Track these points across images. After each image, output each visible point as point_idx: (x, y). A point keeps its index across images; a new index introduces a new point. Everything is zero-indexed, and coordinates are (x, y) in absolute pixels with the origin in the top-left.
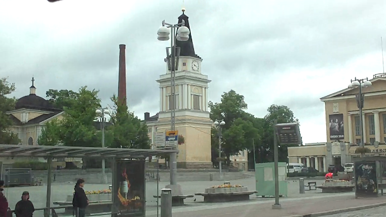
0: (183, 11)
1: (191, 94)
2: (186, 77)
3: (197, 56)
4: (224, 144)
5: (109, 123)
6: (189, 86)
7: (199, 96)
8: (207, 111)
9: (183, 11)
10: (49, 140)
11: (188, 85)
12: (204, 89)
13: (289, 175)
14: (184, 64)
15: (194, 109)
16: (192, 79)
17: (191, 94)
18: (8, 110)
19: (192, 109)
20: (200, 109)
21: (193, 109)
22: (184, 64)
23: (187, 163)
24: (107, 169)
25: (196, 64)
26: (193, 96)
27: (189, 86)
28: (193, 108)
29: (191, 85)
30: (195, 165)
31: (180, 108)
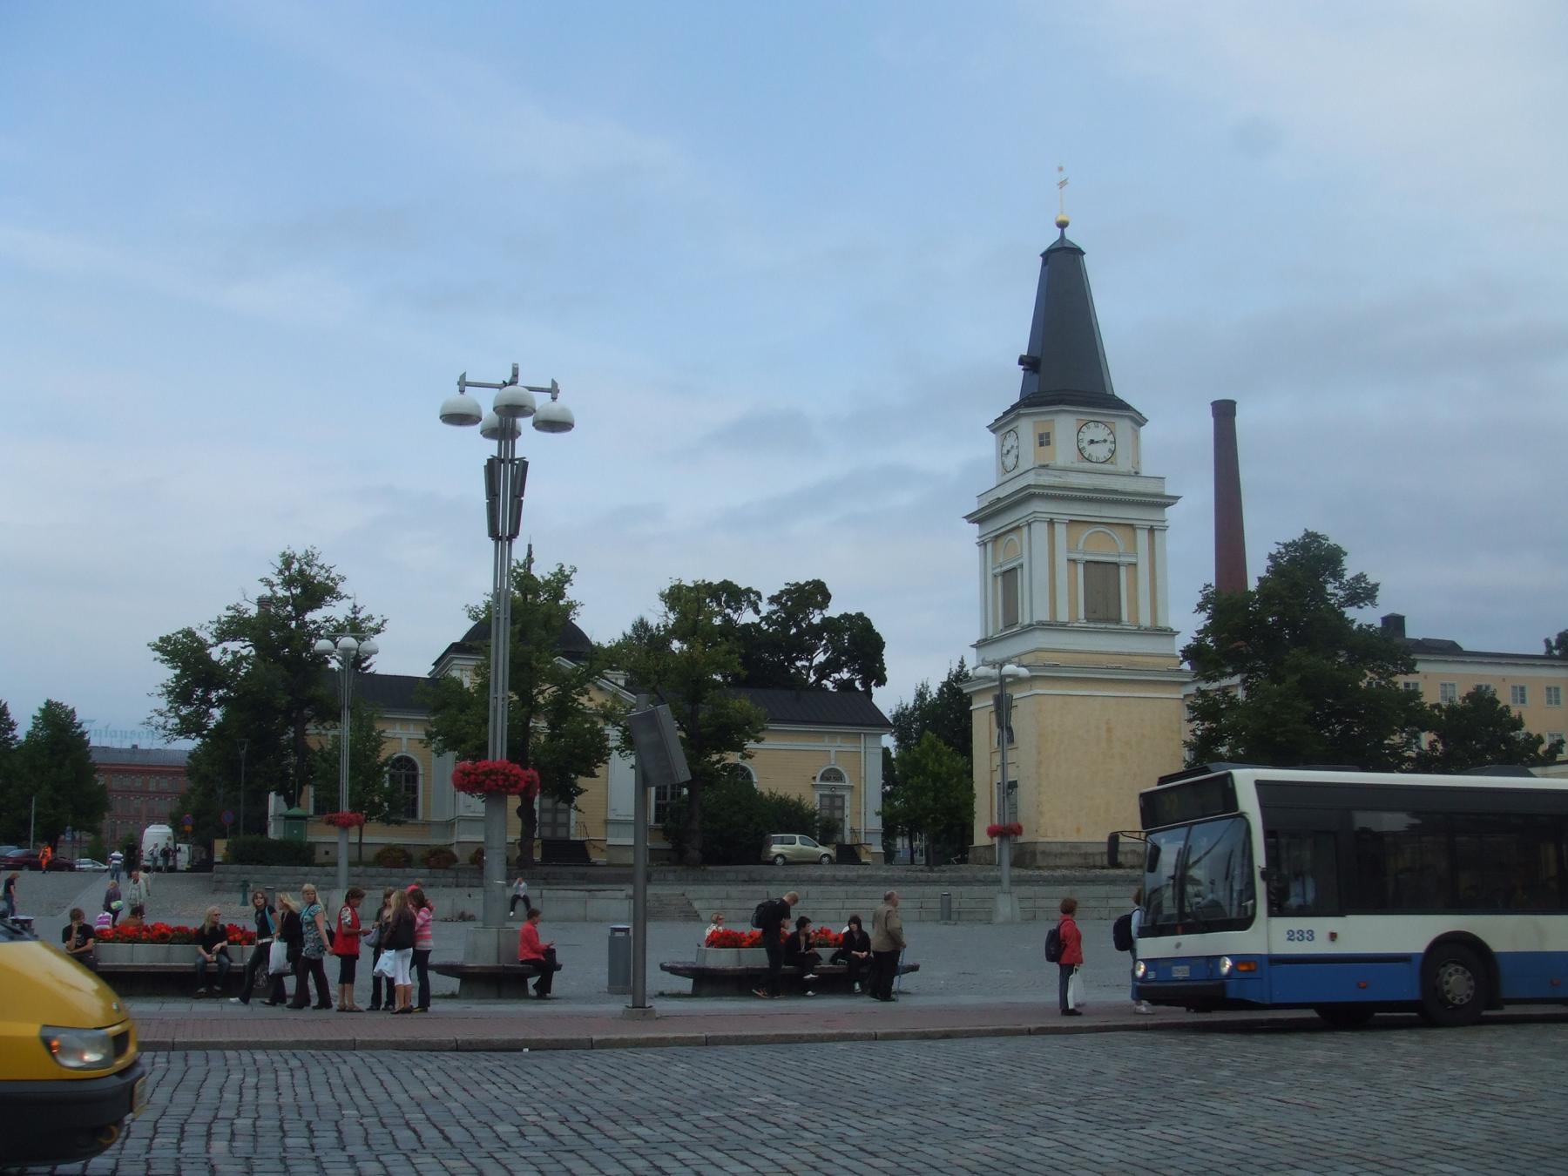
0: (1062, 225)
1: (1072, 561)
2: (1033, 490)
3: (1121, 406)
4: (1326, 737)
5: (14, 751)
6: (1061, 530)
7: (1117, 565)
8: (1161, 624)
9: (1062, 225)
10: (1476, 744)
11: (1051, 522)
12: (1143, 537)
13: (1212, 892)
14: (1044, 440)
15: (1088, 619)
16: (1075, 499)
17: (1072, 561)
18: (1411, 700)
19: (1077, 620)
20: (1125, 616)
21: (1083, 622)
22: (1044, 440)
23: (1040, 848)
24: (1017, 872)
25: (1099, 433)
26: (1080, 568)
27: (1061, 530)
28: (1081, 614)
29: (1071, 521)
30: (1086, 856)
31: (1145, 620)
